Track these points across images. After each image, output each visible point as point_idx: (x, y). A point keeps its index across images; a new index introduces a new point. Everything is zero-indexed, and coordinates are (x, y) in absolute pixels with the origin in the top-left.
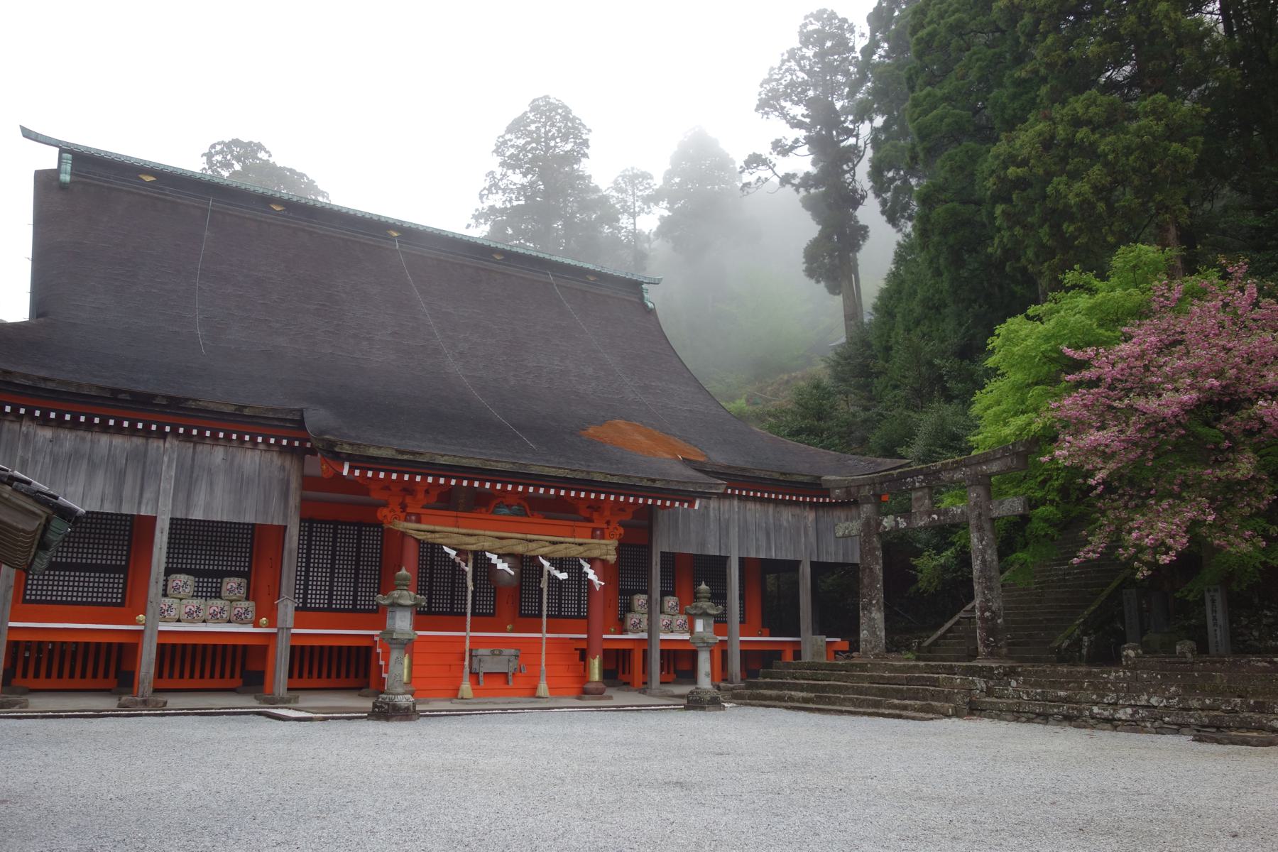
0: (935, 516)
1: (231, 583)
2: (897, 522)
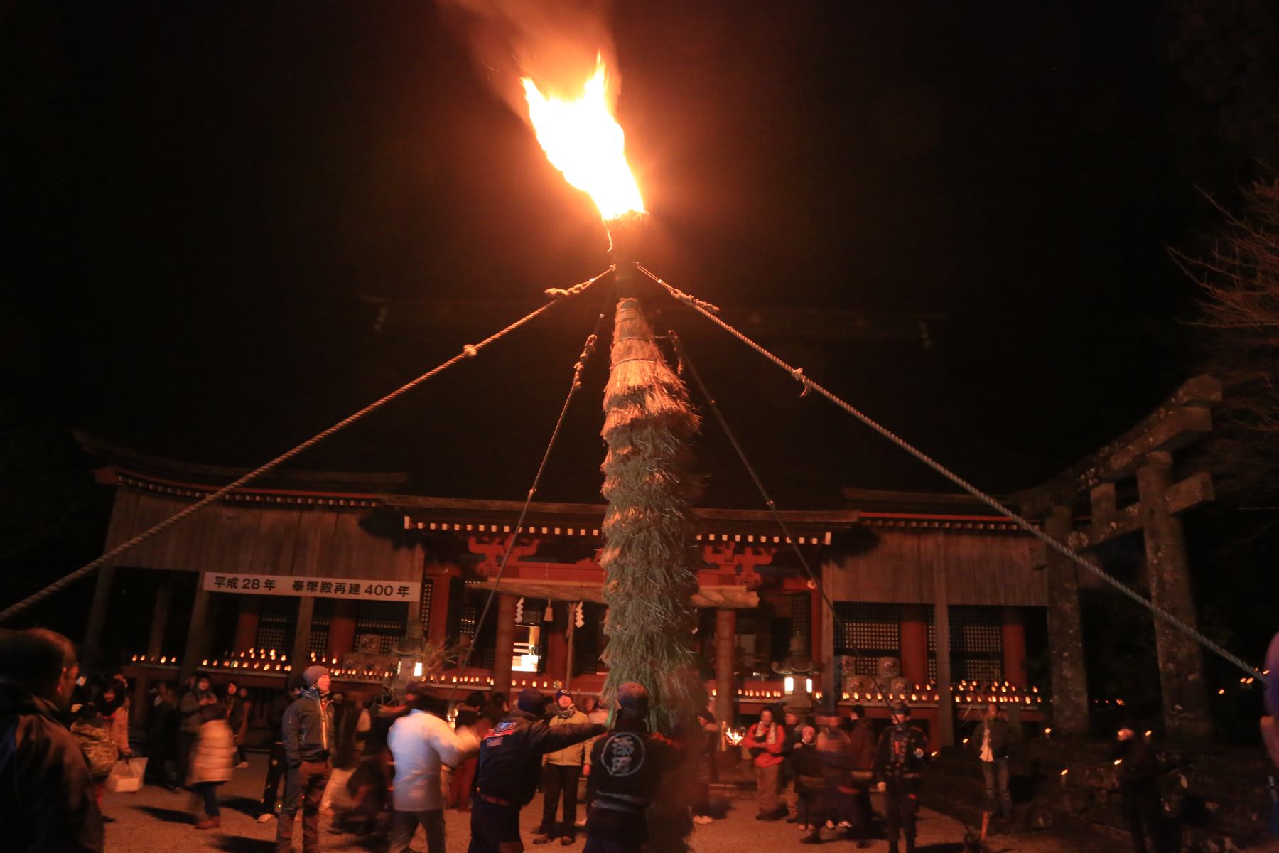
0: (1113, 524)
1: (886, 662)
2: (1079, 538)
